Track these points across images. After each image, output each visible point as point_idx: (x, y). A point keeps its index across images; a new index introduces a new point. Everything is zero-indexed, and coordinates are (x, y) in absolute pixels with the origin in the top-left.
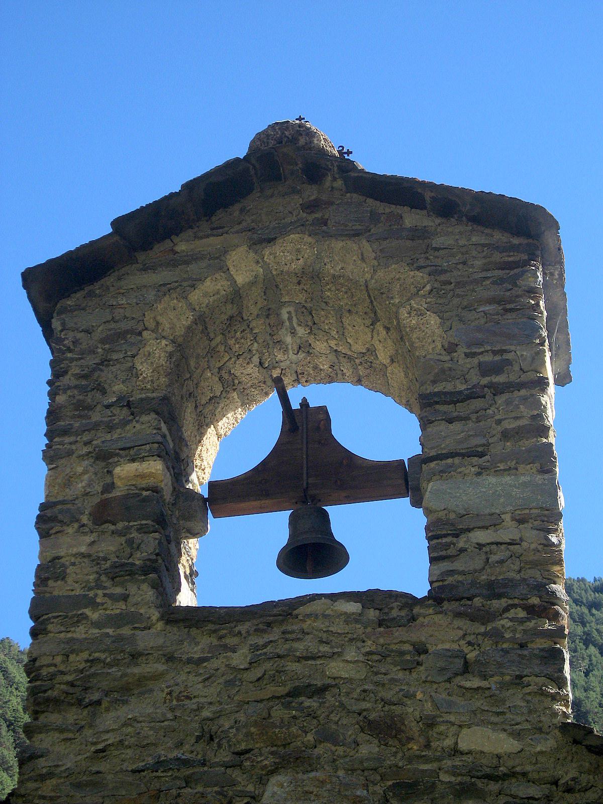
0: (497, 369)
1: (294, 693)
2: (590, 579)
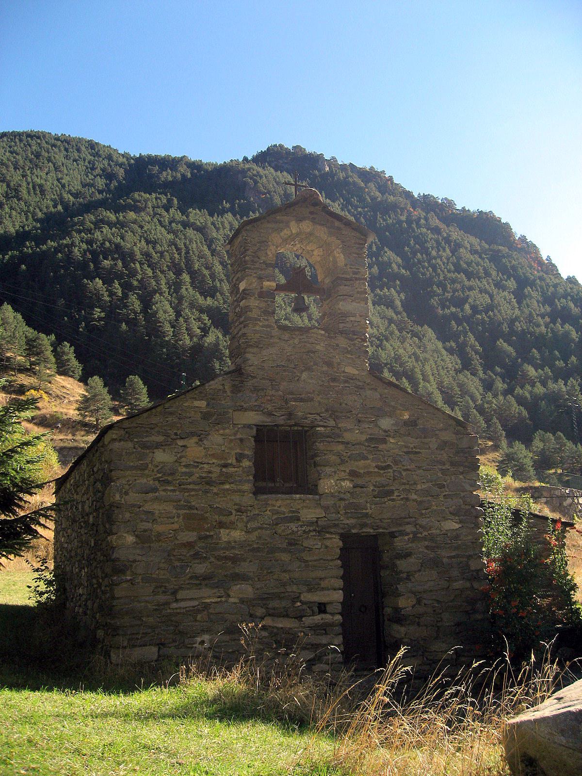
1: (308, 352)
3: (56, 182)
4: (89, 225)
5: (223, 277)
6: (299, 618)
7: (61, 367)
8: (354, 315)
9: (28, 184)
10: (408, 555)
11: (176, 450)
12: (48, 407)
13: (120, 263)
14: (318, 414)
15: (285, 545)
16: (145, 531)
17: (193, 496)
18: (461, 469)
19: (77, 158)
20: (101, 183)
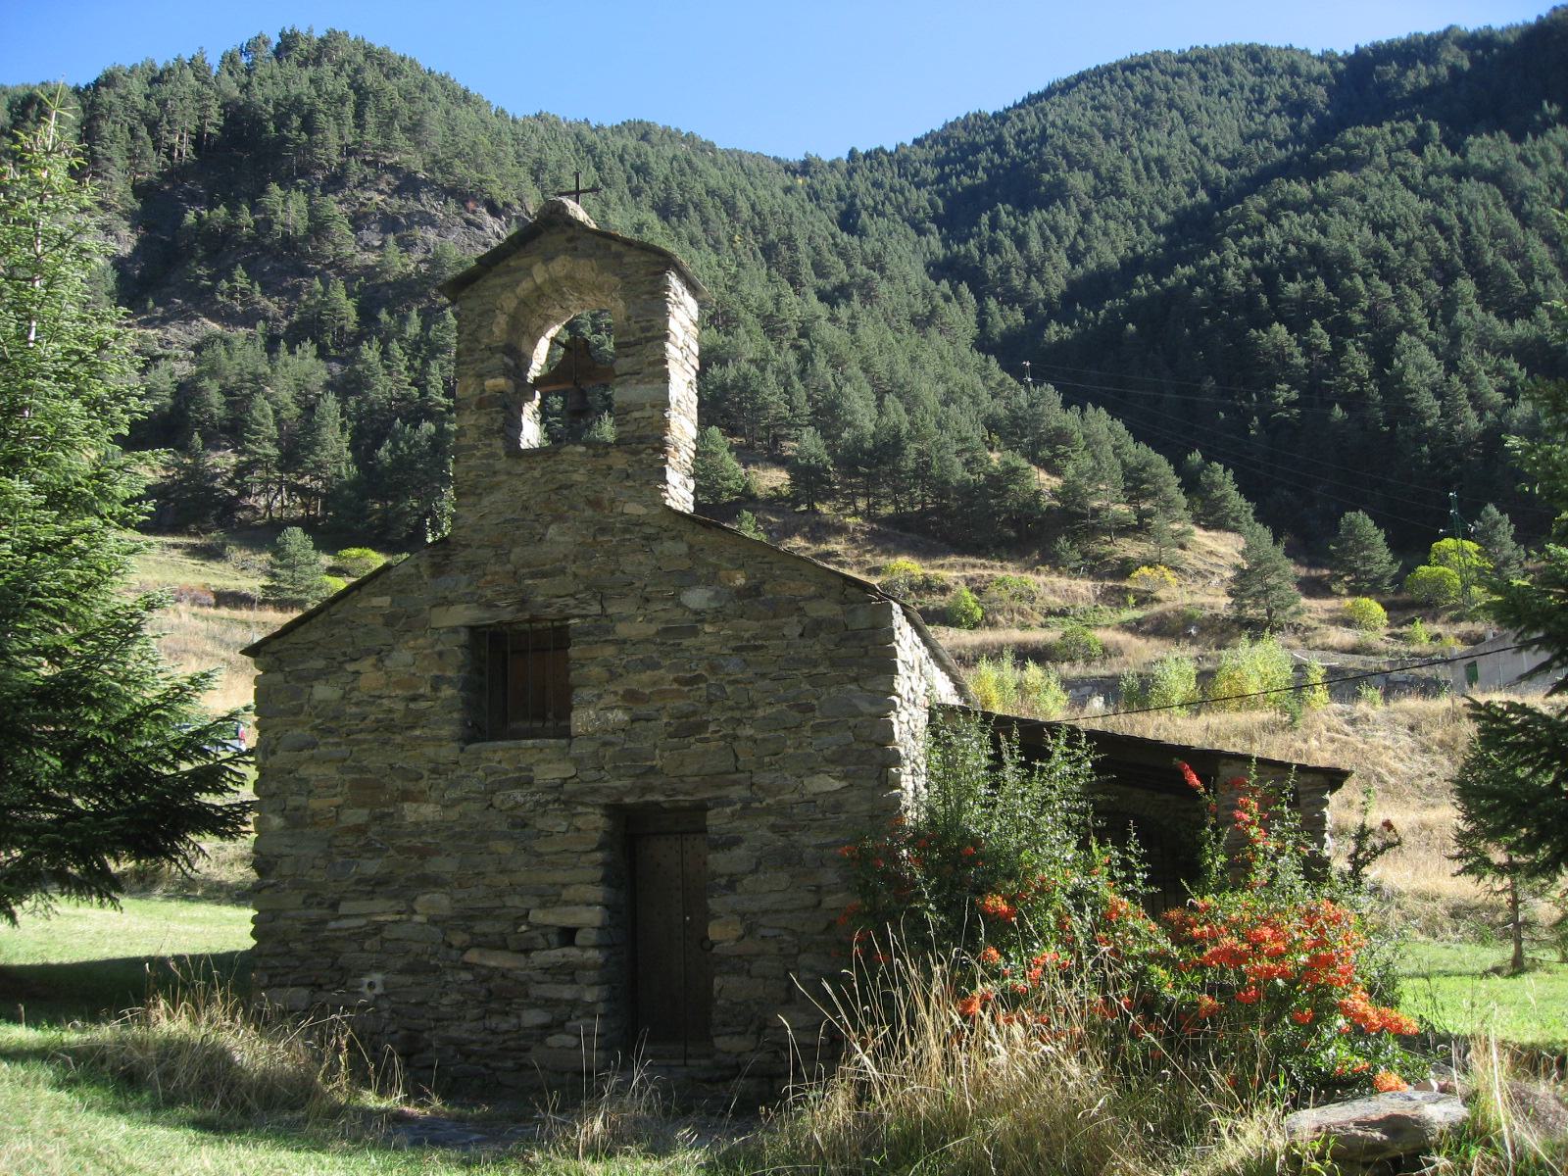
0: (647, 329)
2: (1175, 51)
3: (1189, 146)
4: (1255, 216)
5: (1551, 268)
6: (526, 951)
7: (1212, 514)
8: (642, 407)
9: (1135, 162)
10: (733, 842)
11: (343, 680)
12: (1175, 595)
13: (1320, 284)
14: (572, 596)
15: (504, 827)
16: (297, 809)
17: (365, 750)
18: (853, 672)
19: (1227, 87)
20: (1280, 126)
